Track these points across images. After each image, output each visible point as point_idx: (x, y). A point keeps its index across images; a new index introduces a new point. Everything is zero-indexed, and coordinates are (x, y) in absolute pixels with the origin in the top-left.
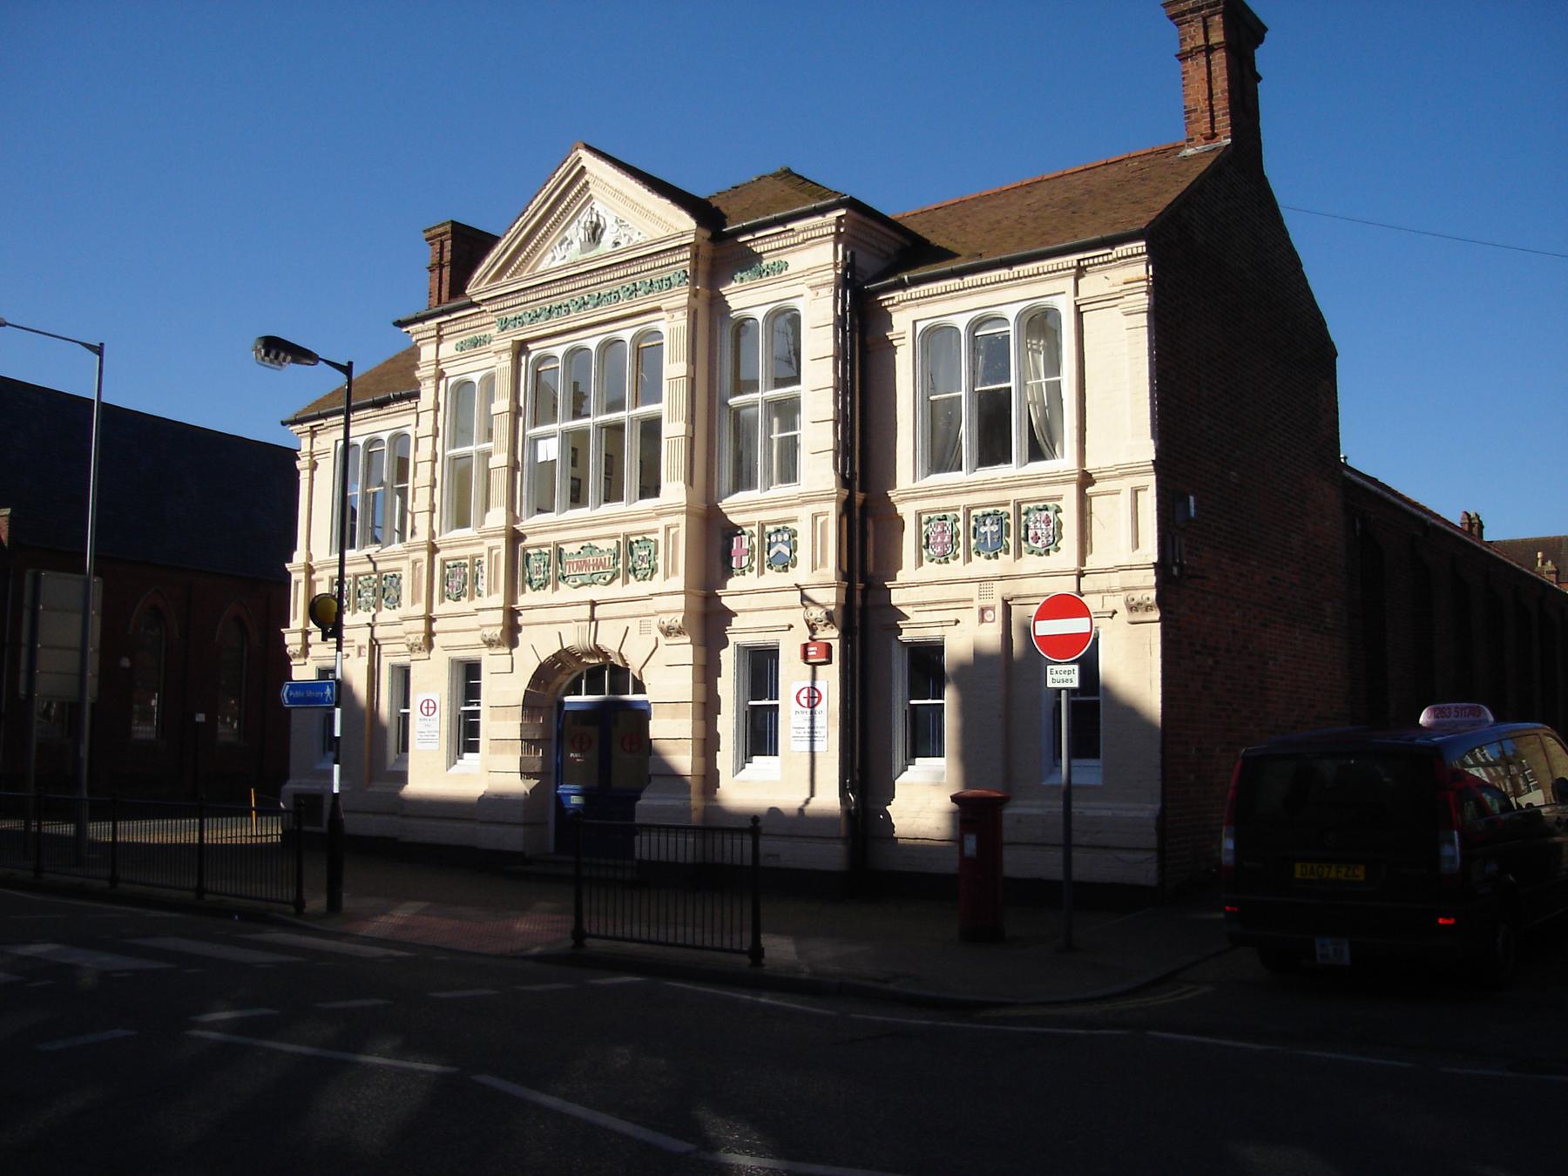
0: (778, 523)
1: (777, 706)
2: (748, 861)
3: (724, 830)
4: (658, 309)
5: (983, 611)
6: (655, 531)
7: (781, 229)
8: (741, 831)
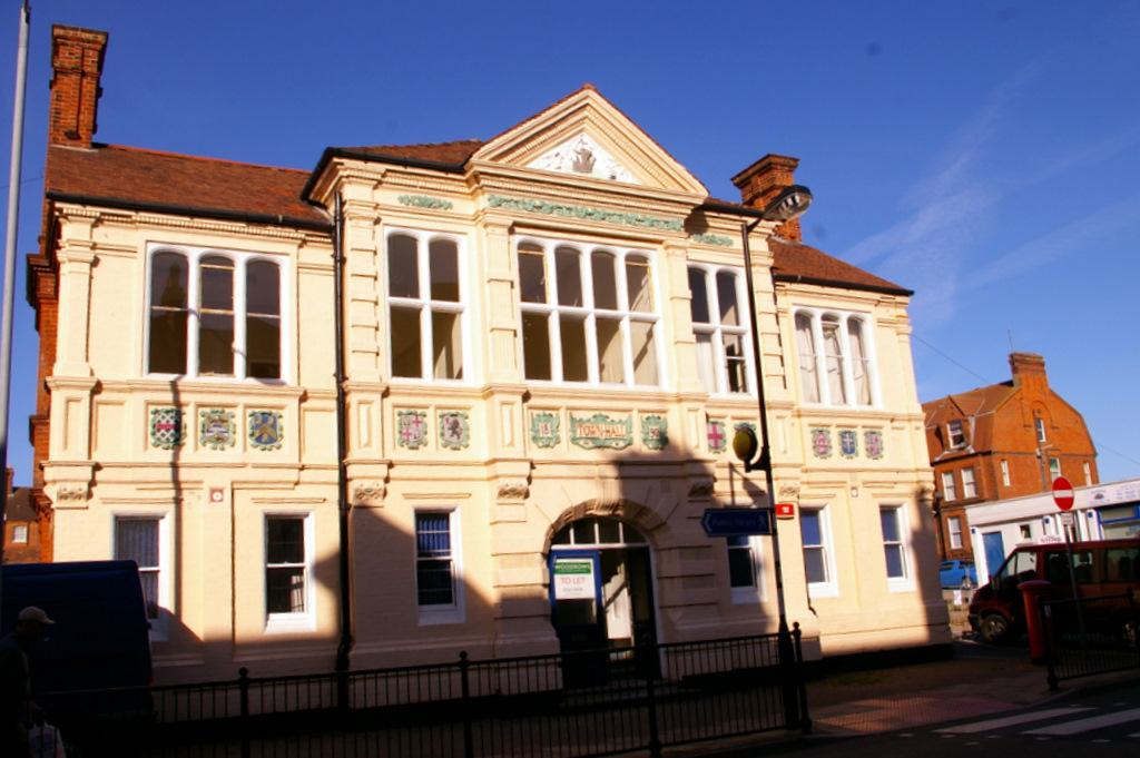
0: (413, 407)
1: (885, 540)
2: (458, 693)
3: (189, 688)
4: (660, 242)
5: (213, 491)
6: (233, 406)
7: (442, 175)
8: (226, 685)
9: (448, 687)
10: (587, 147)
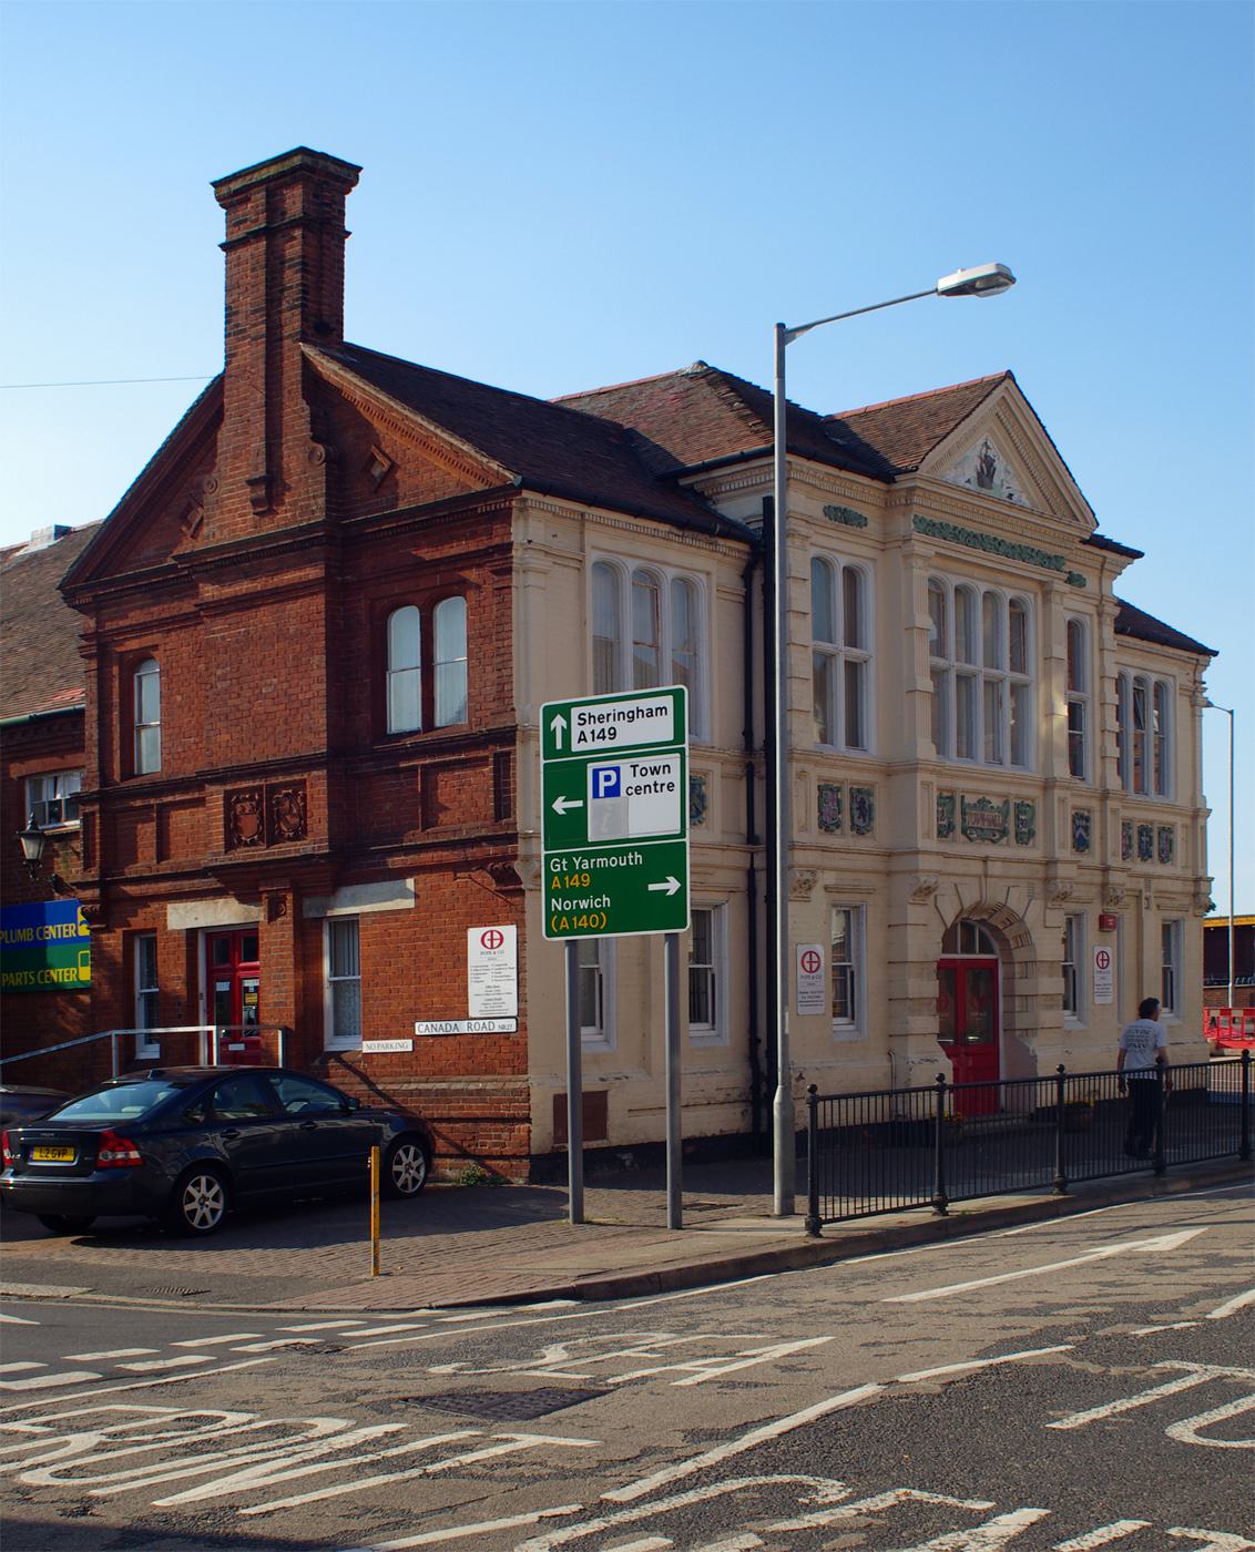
9: (876, 1110)
10: (990, 453)
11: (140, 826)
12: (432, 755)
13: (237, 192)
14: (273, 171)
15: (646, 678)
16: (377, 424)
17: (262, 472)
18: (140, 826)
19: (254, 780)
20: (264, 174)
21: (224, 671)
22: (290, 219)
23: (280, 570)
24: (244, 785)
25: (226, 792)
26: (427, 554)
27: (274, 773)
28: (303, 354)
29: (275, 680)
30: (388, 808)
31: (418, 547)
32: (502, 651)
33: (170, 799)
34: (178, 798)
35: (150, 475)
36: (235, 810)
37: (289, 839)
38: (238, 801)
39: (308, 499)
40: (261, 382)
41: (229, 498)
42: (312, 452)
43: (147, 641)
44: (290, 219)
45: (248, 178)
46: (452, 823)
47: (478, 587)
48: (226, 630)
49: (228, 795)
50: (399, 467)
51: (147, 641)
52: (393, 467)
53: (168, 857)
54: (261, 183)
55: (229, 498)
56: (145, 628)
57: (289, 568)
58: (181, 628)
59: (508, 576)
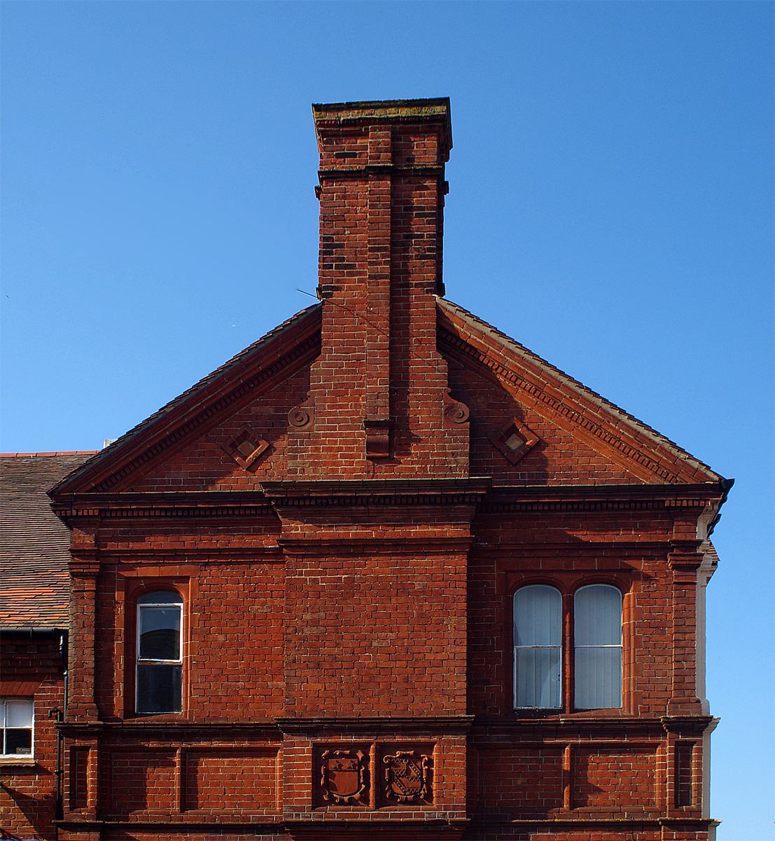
11: (149, 769)
12: (585, 736)
13: (348, 123)
14: (404, 112)
15: (141, 771)
16: (522, 399)
17: (383, 415)
18: (149, 769)
19: (359, 736)
20: (392, 113)
21: (316, 616)
22: (389, 165)
23: (407, 522)
24: (342, 739)
25: (314, 744)
26: (585, 536)
27: (392, 731)
28: (437, 306)
29: (393, 635)
30: (519, 783)
31: (576, 529)
32: (682, 643)
33: (203, 744)
34: (216, 744)
35: (202, 391)
36: (327, 766)
37: (406, 802)
38: (331, 756)
39: (446, 455)
40: (383, 323)
41: (326, 436)
42: (450, 410)
43: (174, 570)
44: (389, 165)
45: (367, 112)
46: (604, 805)
47: (647, 578)
48: (320, 573)
49: (317, 748)
50: (547, 445)
51: (174, 570)
52: (540, 444)
53: (194, 806)
54: (386, 121)
55: (326, 436)
56: (176, 555)
57: (418, 522)
58: (227, 564)
59: (691, 573)
